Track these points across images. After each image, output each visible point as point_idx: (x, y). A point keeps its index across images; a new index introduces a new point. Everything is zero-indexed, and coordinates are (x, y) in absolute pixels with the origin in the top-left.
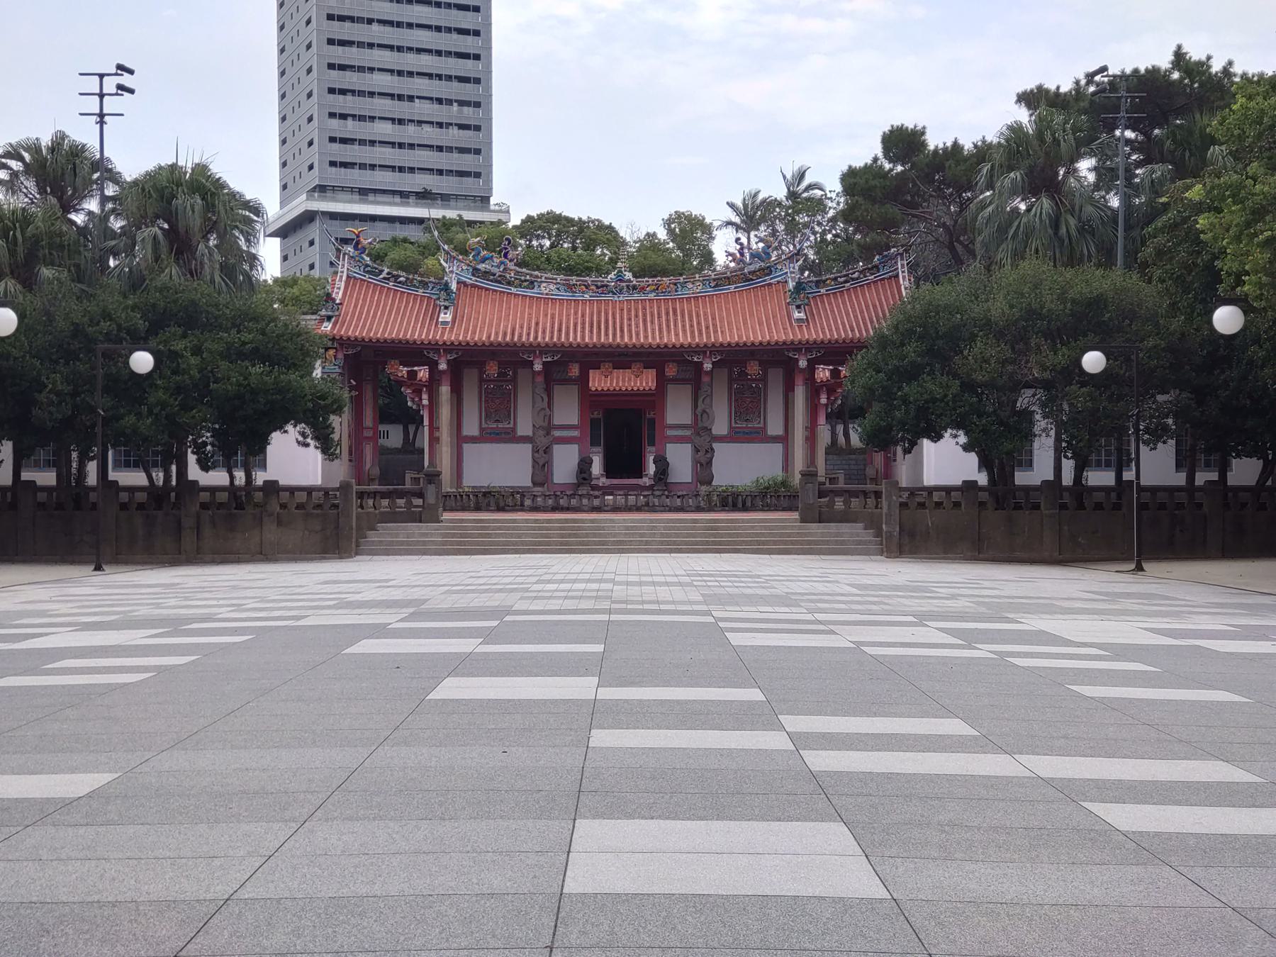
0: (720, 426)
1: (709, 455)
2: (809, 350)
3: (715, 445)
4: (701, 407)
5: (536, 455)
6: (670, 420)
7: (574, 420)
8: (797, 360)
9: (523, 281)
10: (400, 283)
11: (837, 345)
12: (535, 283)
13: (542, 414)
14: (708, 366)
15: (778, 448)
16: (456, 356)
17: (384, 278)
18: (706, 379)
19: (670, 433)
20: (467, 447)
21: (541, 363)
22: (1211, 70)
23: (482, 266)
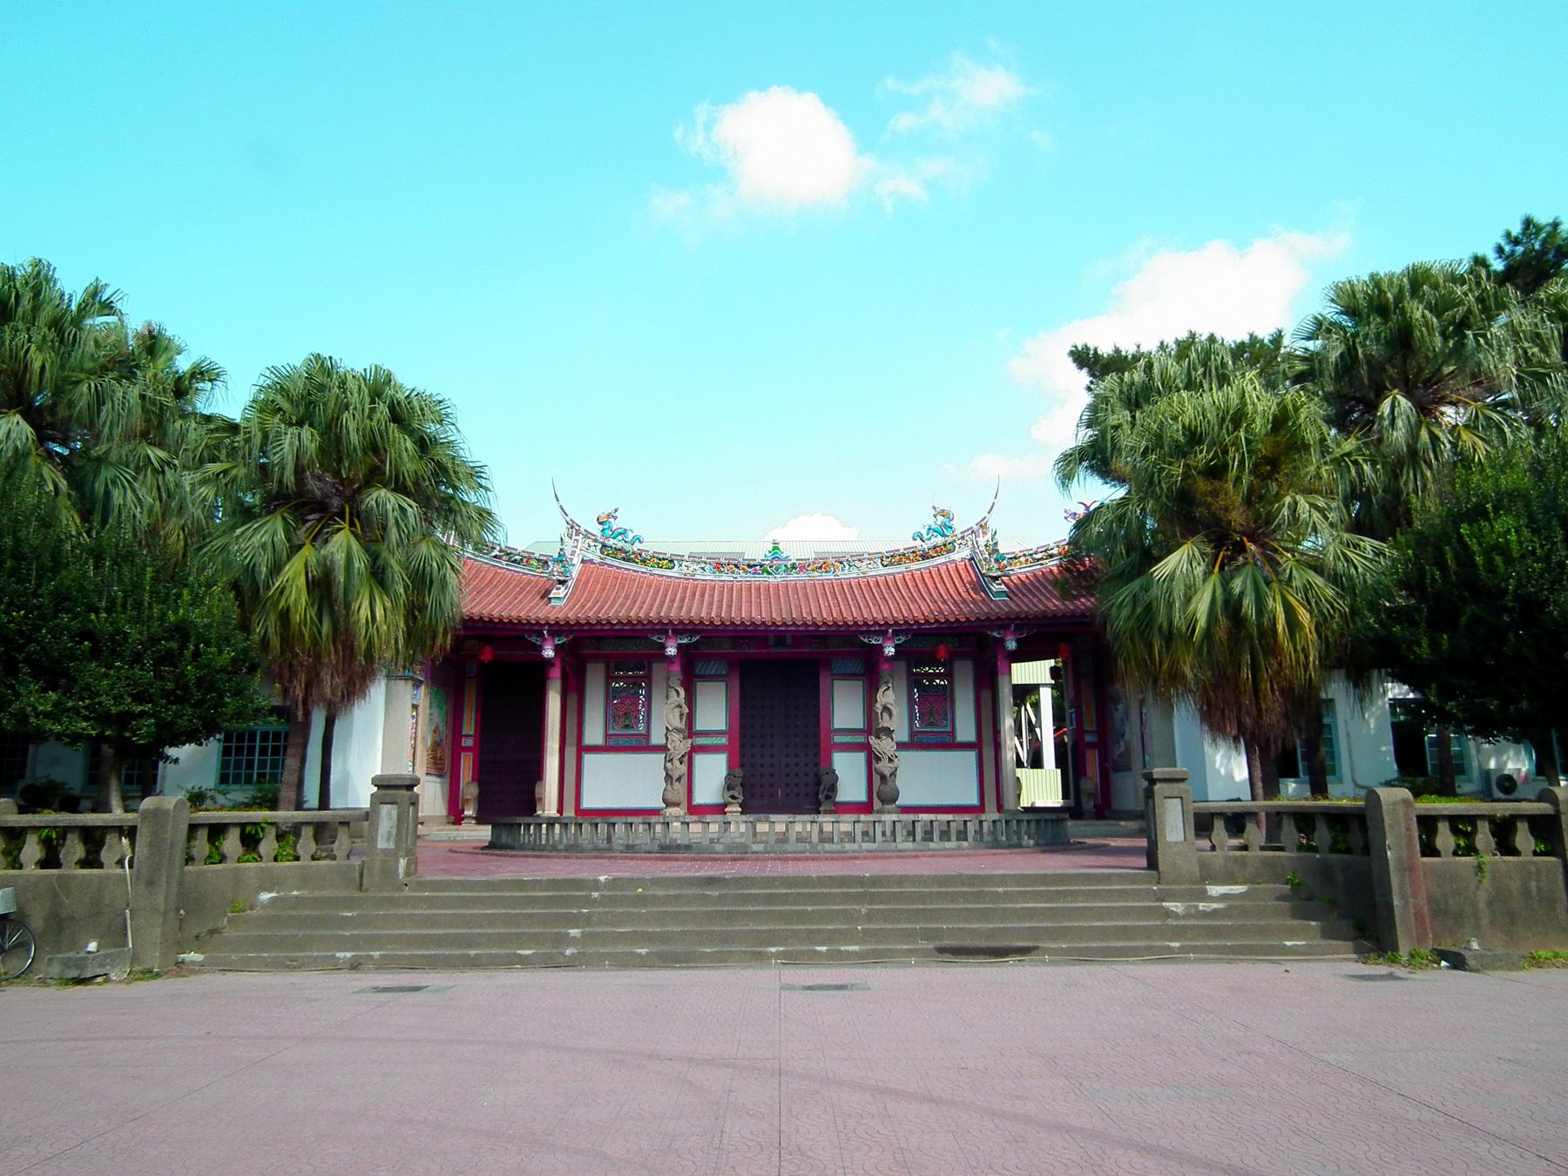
0: (594, 733)
5: (669, 765)
6: (837, 725)
7: (721, 725)
8: (881, 648)
10: (515, 561)
14: (890, 650)
15: (970, 757)
17: (495, 557)
18: (885, 667)
19: (838, 739)
20: (588, 758)
21: (675, 645)
23: (611, 542)
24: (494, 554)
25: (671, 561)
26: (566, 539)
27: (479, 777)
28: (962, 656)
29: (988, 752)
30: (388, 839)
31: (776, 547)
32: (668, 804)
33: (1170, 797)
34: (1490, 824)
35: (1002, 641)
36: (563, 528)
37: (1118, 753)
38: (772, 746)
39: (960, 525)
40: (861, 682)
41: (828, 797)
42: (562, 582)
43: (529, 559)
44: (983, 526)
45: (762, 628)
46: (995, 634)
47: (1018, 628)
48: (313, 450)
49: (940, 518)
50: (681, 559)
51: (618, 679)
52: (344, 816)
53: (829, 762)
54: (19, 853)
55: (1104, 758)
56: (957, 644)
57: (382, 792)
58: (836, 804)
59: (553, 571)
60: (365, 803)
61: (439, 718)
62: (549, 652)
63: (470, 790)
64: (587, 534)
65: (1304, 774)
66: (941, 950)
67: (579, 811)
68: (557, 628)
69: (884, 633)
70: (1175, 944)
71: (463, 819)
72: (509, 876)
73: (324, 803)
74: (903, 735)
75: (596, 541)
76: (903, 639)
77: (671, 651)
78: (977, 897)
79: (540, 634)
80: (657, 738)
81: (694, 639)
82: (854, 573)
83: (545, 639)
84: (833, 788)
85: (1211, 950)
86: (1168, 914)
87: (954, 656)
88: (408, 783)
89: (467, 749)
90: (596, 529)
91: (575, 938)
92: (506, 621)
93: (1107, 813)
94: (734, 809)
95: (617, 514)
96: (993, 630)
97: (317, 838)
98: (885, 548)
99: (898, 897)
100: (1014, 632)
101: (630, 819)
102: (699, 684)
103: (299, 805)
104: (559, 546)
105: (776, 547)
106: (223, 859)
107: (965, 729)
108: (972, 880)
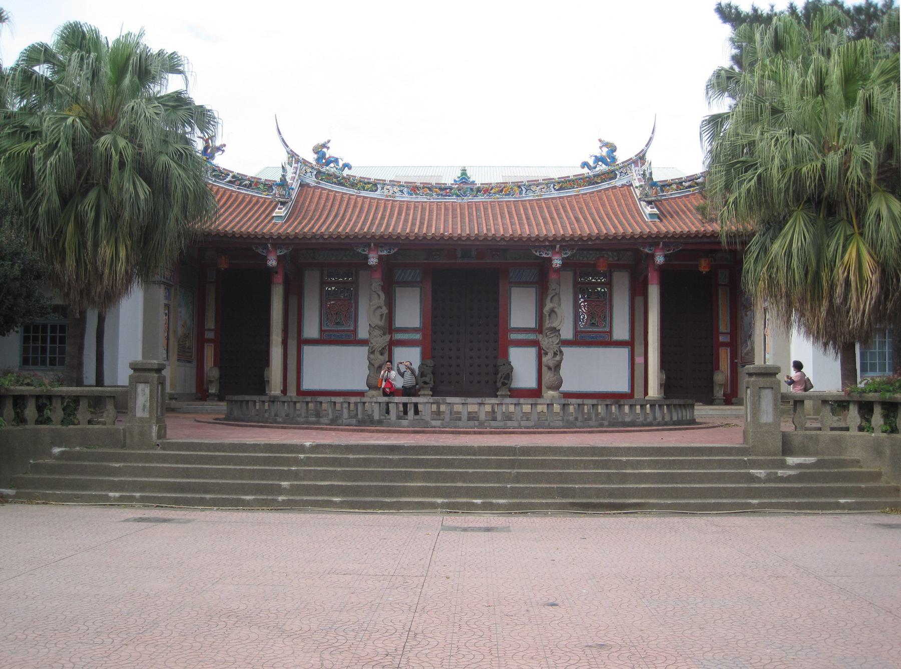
0: (311, 330)
1: (558, 358)
2: (563, 248)
3: (563, 349)
4: (548, 306)
5: (372, 356)
8: (550, 260)
9: (365, 184)
10: (245, 186)
11: (347, 241)
12: (379, 186)
13: (378, 312)
14: (557, 262)
15: (625, 352)
16: (286, 251)
17: (230, 182)
18: (553, 277)
19: (513, 336)
20: (307, 350)
22: (750, 14)
24: (228, 179)
25: (375, 185)
26: (288, 167)
27: (219, 361)
28: (621, 267)
29: (639, 349)
30: (144, 410)
31: (464, 172)
32: (371, 386)
33: (764, 388)
34: (883, 409)
35: (652, 256)
36: (284, 157)
37: (745, 351)
38: (458, 342)
39: (622, 156)
40: (534, 290)
41: (504, 384)
42: (283, 203)
43: (256, 185)
44: (641, 158)
45: (321, 241)
46: (647, 250)
47: (666, 245)
48: (852, 130)
49: (605, 150)
50: (384, 183)
51: (331, 284)
52: (110, 392)
53: (506, 355)
54: (38, 418)
55: (734, 355)
56: (616, 258)
57: (137, 374)
58: (511, 390)
59: (275, 194)
60: (126, 382)
61: (184, 314)
62: (272, 262)
63: (212, 372)
64: (305, 162)
65: (889, 370)
66: (573, 505)
67: (301, 393)
68: (279, 241)
69: (554, 247)
70: (479, 501)
71: (208, 396)
72: (236, 441)
73: (100, 381)
74: (567, 333)
75: (312, 168)
76: (569, 253)
77: (373, 260)
78: (605, 464)
79: (266, 247)
80: (363, 334)
81: (393, 252)
82: (530, 196)
83: (268, 251)
84: (508, 376)
85: (669, 506)
86: (753, 479)
87: (612, 268)
88: (156, 367)
89: (209, 341)
90: (311, 158)
91: (285, 489)
92: (245, 236)
93: (734, 400)
94: (426, 392)
95: (329, 145)
96: (645, 247)
97: (15, 405)
98: (556, 175)
99: (543, 464)
100: (663, 249)
101: (334, 399)
102: (397, 289)
103: (79, 383)
104: (281, 172)
105: (464, 172)
106: (48, 421)
107: (621, 331)
108: (594, 451)
